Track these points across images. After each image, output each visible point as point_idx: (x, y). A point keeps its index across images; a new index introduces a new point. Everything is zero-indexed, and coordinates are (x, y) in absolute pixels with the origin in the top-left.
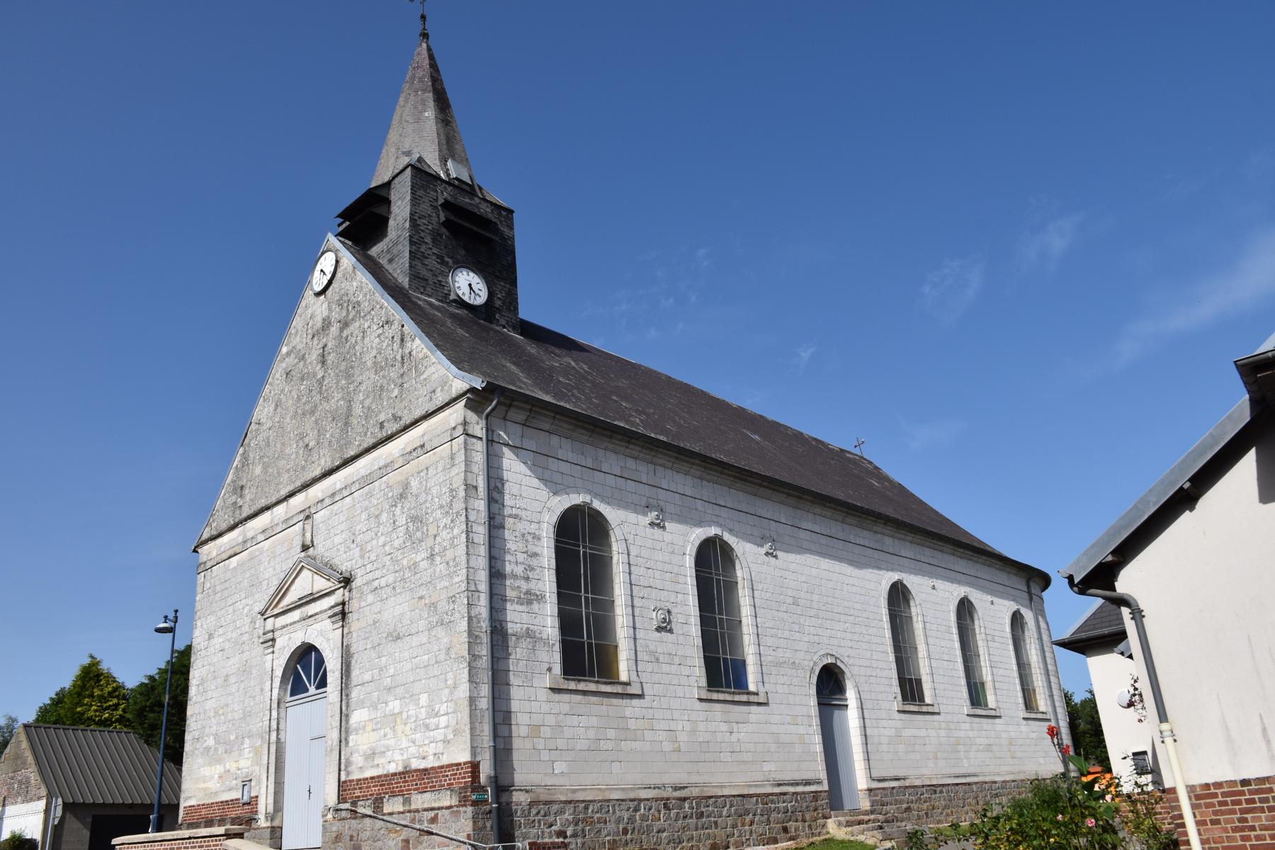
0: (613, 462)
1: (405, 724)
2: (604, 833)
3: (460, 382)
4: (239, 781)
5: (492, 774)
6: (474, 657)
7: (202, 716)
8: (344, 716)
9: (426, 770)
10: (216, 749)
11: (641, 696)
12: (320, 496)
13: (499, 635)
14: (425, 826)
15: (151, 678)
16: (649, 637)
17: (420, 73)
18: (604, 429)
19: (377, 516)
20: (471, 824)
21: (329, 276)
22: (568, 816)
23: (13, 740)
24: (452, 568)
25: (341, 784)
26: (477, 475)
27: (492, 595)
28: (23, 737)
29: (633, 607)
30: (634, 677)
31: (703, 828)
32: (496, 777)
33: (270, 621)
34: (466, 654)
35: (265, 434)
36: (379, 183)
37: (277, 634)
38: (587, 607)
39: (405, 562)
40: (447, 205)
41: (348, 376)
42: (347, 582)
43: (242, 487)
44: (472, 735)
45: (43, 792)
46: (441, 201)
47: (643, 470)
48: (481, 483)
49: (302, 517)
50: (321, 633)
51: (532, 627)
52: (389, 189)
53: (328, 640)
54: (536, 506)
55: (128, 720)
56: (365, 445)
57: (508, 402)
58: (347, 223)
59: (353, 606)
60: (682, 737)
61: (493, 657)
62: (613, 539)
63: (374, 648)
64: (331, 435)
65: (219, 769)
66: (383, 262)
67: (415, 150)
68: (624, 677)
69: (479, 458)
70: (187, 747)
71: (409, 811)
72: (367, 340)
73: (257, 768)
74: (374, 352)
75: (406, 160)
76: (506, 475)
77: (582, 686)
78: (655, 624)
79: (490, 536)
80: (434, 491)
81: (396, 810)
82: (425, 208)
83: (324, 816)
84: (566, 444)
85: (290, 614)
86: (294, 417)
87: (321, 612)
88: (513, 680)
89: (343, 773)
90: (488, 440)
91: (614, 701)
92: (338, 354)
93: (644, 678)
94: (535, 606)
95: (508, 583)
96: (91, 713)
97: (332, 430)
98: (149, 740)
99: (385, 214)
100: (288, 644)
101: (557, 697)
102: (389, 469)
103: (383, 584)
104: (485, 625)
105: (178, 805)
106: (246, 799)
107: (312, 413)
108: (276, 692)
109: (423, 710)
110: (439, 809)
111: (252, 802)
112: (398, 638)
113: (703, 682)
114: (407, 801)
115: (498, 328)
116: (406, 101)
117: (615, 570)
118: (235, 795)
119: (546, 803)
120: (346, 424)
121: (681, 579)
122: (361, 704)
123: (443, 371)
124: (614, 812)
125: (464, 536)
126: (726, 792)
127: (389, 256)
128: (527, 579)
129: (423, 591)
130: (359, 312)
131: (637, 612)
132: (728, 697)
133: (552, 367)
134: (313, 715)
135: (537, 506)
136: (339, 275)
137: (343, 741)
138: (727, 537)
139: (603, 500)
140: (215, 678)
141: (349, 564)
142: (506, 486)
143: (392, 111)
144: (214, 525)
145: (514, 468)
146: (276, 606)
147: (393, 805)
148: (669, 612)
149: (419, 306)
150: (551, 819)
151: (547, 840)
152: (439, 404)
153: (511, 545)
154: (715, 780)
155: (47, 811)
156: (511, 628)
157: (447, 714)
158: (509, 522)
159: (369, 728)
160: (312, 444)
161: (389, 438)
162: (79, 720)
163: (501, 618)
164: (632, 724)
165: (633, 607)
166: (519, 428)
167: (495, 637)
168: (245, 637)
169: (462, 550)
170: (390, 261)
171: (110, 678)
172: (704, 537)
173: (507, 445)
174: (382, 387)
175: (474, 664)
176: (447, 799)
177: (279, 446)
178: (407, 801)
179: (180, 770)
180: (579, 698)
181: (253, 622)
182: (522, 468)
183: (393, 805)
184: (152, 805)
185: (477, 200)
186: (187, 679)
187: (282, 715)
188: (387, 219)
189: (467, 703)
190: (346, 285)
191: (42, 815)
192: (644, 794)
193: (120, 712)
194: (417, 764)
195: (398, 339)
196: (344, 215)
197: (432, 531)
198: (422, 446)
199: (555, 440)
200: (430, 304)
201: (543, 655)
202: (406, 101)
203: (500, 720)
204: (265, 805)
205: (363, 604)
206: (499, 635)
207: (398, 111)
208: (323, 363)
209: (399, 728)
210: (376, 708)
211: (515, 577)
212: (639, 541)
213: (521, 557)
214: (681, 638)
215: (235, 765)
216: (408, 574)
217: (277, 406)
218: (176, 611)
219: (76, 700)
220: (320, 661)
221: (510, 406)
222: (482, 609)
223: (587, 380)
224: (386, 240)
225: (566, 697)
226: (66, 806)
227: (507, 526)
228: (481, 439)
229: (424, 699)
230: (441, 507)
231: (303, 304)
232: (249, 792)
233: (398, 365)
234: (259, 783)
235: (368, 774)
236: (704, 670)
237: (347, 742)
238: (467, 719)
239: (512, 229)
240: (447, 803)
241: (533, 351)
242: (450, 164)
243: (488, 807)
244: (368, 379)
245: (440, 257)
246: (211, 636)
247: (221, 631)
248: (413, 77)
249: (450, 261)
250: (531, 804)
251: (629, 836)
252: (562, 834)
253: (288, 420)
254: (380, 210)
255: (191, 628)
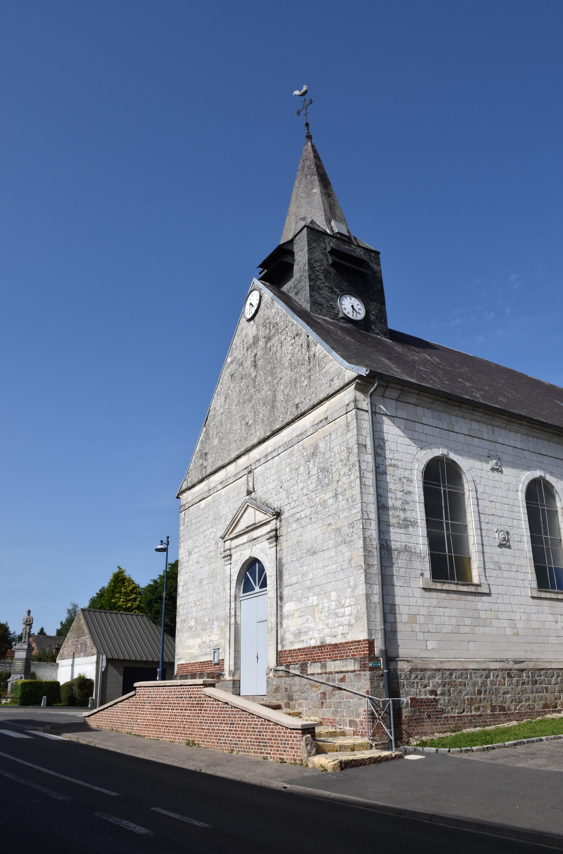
0: (462, 424)
1: (321, 613)
2: (464, 693)
3: (350, 372)
4: (212, 648)
5: (383, 648)
6: (368, 566)
7: (187, 606)
8: (279, 608)
9: (336, 645)
10: (196, 628)
11: (489, 594)
12: (258, 457)
13: (385, 550)
14: (337, 684)
15: (155, 581)
16: (493, 551)
17: (308, 163)
18: (456, 401)
19: (297, 469)
20: (369, 683)
21: (256, 307)
22: (438, 680)
23: (76, 619)
24: (350, 503)
25: (278, 653)
26: (366, 437)
27: (379, 522)
28: (81, 617)
29: (481, 529)
30: (483, 581)
31: (537, 692)
32: (386, 651)
33: (228, 543)
34: (362, 563)
35: (219, 418)
36: (286, 241)
37: (233, 551)
38: (448, 530)
39: (317, 500)
40: (333, 252)
41: (272, 373)
42: (278, 515)
43: (206, 454)
44: (368, 620)
45: (95, 651)
46: (329, 249)
47: (485, 430)
48: (369, 443)
49: (246, 472)
50: (262, 550)
51: (408, 545)
52: (292, 245)
53: (267, 555)
54: (408, 458)
55: (143, 608)
56: (287, 421)
57: (385, 384)
58: (266, 271)
59: (283, 531)
60: (520, 625)
61: (381, 566)
62: (465, 481)
63: (298, 560)
64: (263, 415)
65: (199, 641)
66: (292, 295)
67: (308, 216)
68: (476, 580)
69: (367, 425)
70: (178, 626)
71: (326, 673)
72: (284, 348)
73: (222, 641)
74: (289, 356)
75: (303, 224)
76: (386, 437)
77: (446, 587)
78: (497, 542)
79: (377, 480)
80: (336, 449)
81: (316, 672)
82: (318, 255)
83: (267, 674)
84: (428, 413)
85: (240, 538)
86: (237, 405)
87: (261, 536)
88: (396, 582)
89: (279, 646)
90: (372, 412)
91: (469, 598)
92: (265, 359)
93: (491, 581)
94: (411, 529)
95: (391, 513)
96: (120, 603)
97: (263, 411)
98: (155, 620)
99: (291, 262)
100: (240, 557)
101: (428, 594)
102: (304, 436)
103: (303, 516)
104: (375, 543)
105: (174, 663)
106: (216, 661)
107: (250, 401)
108: (233, 590)
109: (334, 603)
110: (346, 672)
111: (220, 663)
112: (314, 553)
113: (535, 584)
114: (324, 666)
115: (375, 335)
116: (300, 184)
117: (467, 503)
118: (209, 658)
119: (422, 670)
120: (273, 407)
121: (516, 509)
122: (291, 599)
123: (338, 365)
124: (471, 678)
125: (358, 480)
126: (554, 666)
127: (295, 291)
128: (404, 510)
129: (331, 520)
130: (277, 330)
131: (484, 533)
132: (553, 596)
133: (414, 360)
134: (259, 605)
135: (409, 458)
136: (262, 305)
137: (279, 624)
138: (548, 478)
139: (456, 452)
140: (194, 581)
141: (279, 503)
142: (387, 444)
143: (292, 190)
144: (189, 480)
145: (391, 431)
146: (231, 533)
147: (314, 669)
148: (508, 533)
149: (319, 323)
150: (426, 682)
151: (423, 697)
152: (337, 388)
153: (391, 486)
154: (545, 657)
155: (98, 663)
156: (394, 545)
157: (350, 606)
158: (390, 470)
159: (296, 615)
160: (250, 422)
161: (303, 415)
162: (113, 607)
163: (387, 538)
164: (483, 614)
165: (481, 529)
166: (394, 402)
167: (383, 552)
168: (212, 554)
169: (357, 490)
170: (297, 294)
171: (131, 581)
172: (531, 478)
173: (386, 415)
174: (296, 379)
175: (368, 571)
176: (351, 666)
177: (229, 425)
178: (324, 666)
179: (174, 641)
180: (444, 595)
181: (217, 543)
182: (398, 431)
183: (314, 669)
184: (158, 662)
185: (354, 247)
186: (177, 582)
187: (238, 606)
188: (292, 265)
189: (364, 598)
190: (267, 312)
191: (95, 665)
192: (493, 666)
193: (137, 603)
194: (330, 641)
195: (305, 346)
196: (263, 265)
197: (336, 478)
198: (326, 419)
199: (420, 410)
200: (326, 321)
201: (417, 564)
202: (300, 184)
203: (387, 610)
204: (228, 665)
205: (289, 530)
206: (385, 550)
207: (295, 191)
208: (255, 366)
209: (317, 615)
210: (301, 601)
211: (395, 509)
212: (484, 482)
213: (399, 495)
214: (517, 552)
215: (208, 638)
216: (320, 508)
217: (226, 398)
218: (168, 538)
219: (111, 595)
220: (262, 570)
221: (387, 387)
222: (373, 531)
223: (439, 368)
224: (293, 280)
225: (434, 594)
226: (108, 660)
227: (388, 472)
228: (367, 411)
229: (334, 595)
230: (342, 460)
231: (240, 328)
232: (218, 656)
233: (306, 363)
234: (224, 651)
235: (296, 647)
236: (535, 575)
237: (282, 625)
238: (364, 610)
239: (379, 264)
240: (352, 668)
241: (400, 350)
242: (333, 223)
243: (381, 672)
244: (286, 375)
245: (331, 289)
246: (190, 553)
247: (196, 550)
248: (304, 166)
249: (338, 290)
250: (411, 671)
251: (482, 696)
252: (433, 692)
253: (234, 407)
254: (288, 259)
255: (177, 548)
